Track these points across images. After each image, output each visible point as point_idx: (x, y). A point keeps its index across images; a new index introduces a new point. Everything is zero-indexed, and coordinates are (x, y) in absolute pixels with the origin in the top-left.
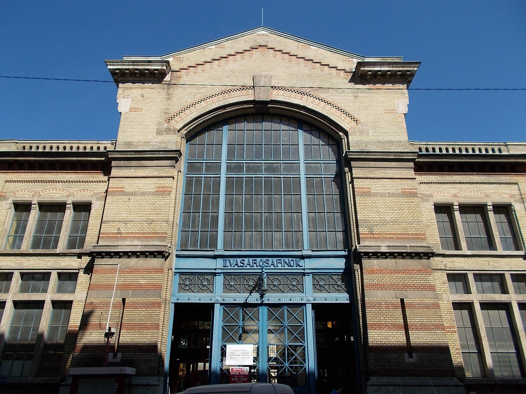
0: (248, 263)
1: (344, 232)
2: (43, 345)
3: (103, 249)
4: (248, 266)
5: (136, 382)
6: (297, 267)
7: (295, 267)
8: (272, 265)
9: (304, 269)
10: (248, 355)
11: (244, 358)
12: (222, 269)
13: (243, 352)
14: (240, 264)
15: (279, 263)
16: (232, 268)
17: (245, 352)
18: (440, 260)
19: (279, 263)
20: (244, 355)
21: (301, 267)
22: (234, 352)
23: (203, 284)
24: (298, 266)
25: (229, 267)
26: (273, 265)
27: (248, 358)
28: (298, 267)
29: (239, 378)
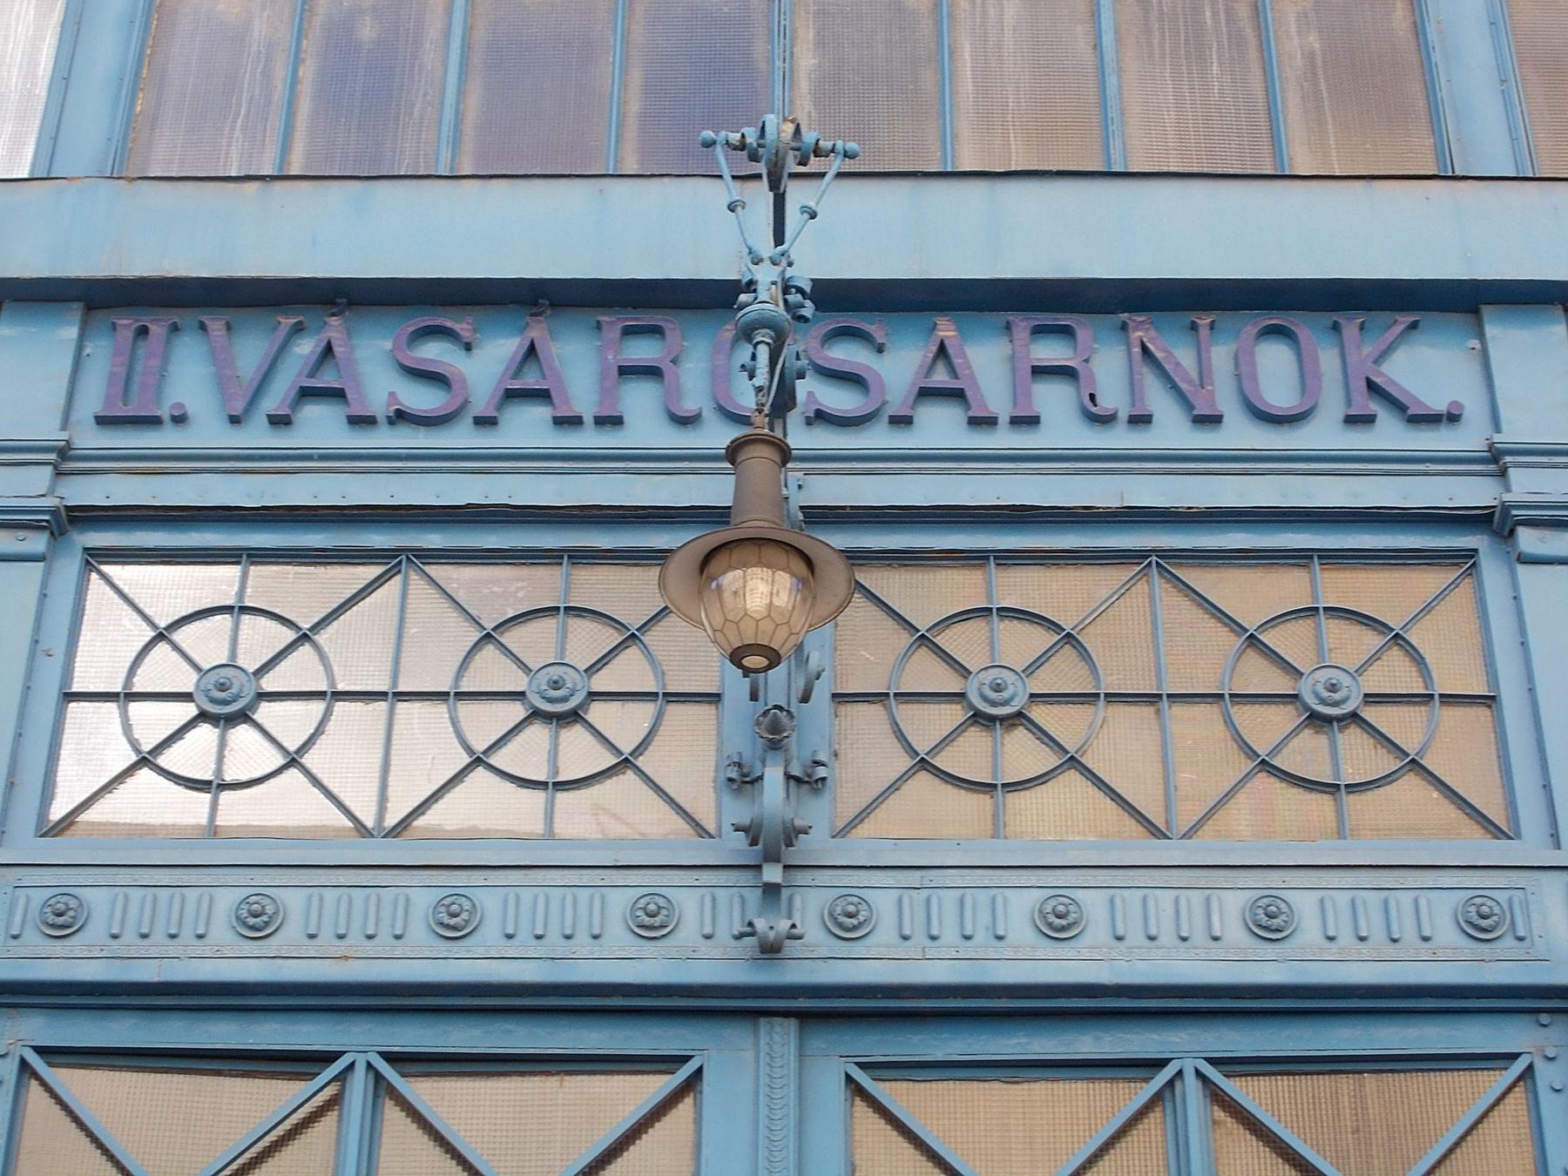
0: (940, 378)
1: (1486, 311)
2: (1299, 61)
3: (1047, 319)
4: (314, 412)
5: (1114, 139)
6: (1358, 421)
7: (1324, 434)
8: (927, 394)
9: (1496, 461)
12: (64, 459)
15: (1039, 372)
16: (257, 436)
18: (778, 1112)
19: (1039, 372)
21: (1431, 420)
23: (1305, 690)
24: (1385, 417)
25: (209, 433)
26: (956, 395)
28: (1389, 435)
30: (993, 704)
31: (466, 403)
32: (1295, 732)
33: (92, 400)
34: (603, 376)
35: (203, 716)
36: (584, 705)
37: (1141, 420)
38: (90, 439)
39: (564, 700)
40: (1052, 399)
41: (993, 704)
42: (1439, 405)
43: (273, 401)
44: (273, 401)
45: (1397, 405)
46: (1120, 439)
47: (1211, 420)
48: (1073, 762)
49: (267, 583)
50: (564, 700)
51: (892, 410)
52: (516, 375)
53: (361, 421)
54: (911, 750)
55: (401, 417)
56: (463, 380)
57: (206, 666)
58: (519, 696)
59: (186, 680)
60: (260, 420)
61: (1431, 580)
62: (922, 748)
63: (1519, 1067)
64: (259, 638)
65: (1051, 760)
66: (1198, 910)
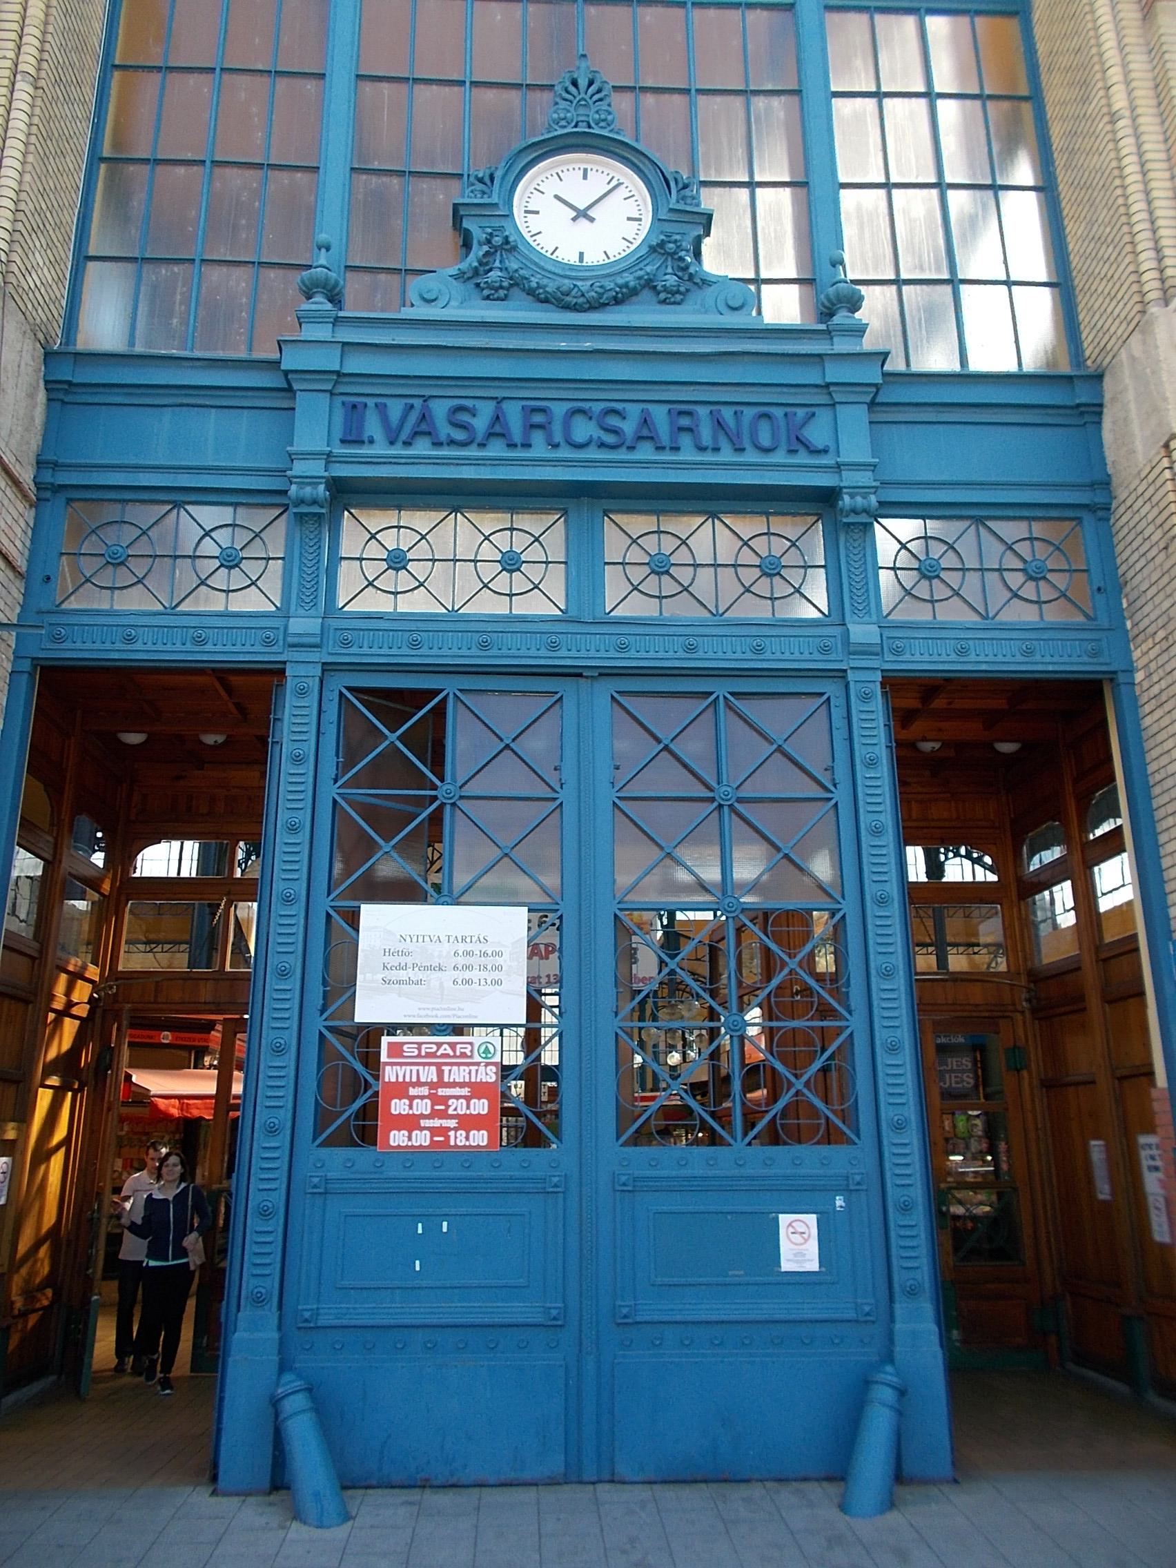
6: (792, 452)
8: (640, 438)
9: (838, 467)
10: (498, 968)
11: (468, 982)
12: (329, 458)
13: (461, 947)
14: (445, 430)
17: (476, 948)
20: (468, 967)
22: (411, 947)
24: (803, 452)
27: (497, 982)
28: (803, 458)
29: (435, 1099)
30: (930, 571)
31: (474, 438)
32: (115, 572)
33: (338, 433)
34: (525, 427)
35: (222, 565)
36: (126, 560)
37: (717, 450)
38: (339, 450)
39: (233, 560)
40: (685, 440)
41: (930, 571)
42: (821, 447)
43: (404, 436)
44: (404, 436)
45: (807, 447)
46: (708, 457)
47: (741, 450)
48: (686, 589)
49: (243, 517)
50: (233, 560)
51: (628, 443)
52: (418, 426)
53: (437, 444)
54: (483, 582)
55: (452, 442)
56: (473, 427)
57: (224, 547)
58: (1025, 561)
59: (217, 552)
60: (400, 444)
61: (1068, 525)
62: (747, 585)
63: (825, 697)
64: (242, 537)
65: (950, 593)
66: (583, 641)
